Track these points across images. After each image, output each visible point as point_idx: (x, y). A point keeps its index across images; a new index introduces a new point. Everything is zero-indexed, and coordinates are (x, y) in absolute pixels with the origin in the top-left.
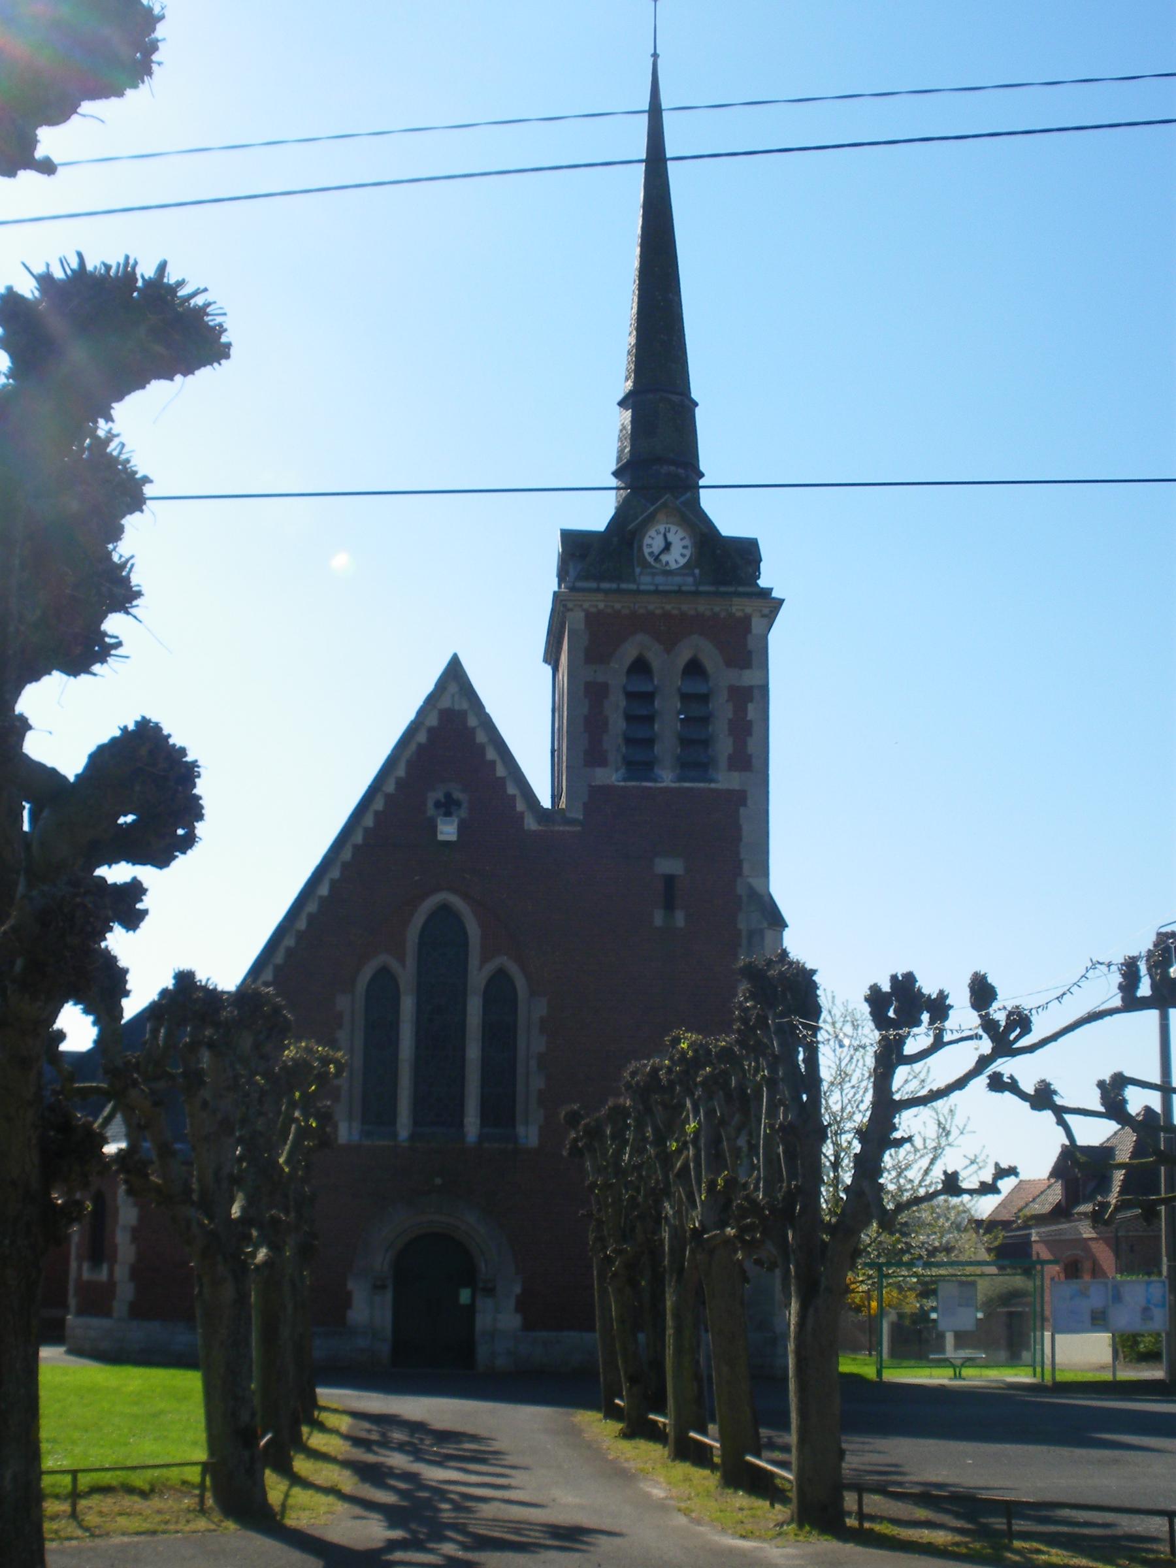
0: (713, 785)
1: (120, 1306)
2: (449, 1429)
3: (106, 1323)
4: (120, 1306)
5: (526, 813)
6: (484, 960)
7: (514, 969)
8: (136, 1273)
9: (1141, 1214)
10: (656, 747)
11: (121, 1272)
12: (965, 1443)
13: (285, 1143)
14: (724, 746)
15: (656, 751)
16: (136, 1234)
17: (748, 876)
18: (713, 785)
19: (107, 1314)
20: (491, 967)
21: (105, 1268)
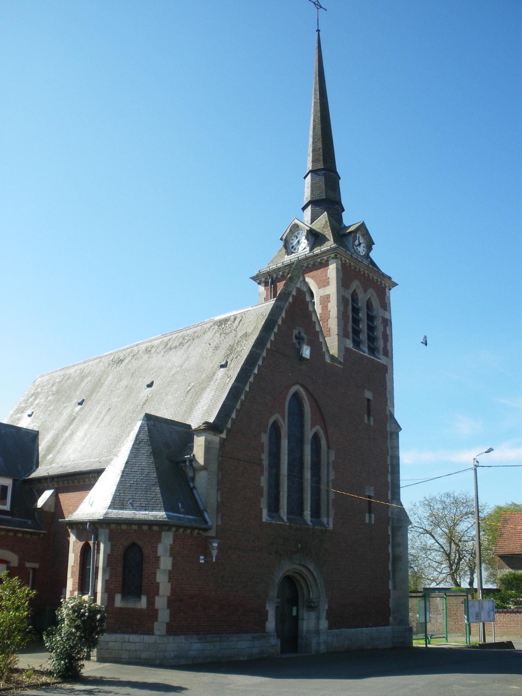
0: (379, 360)
1: (160, 627)
2: (141, 689)
3: (147, 639)
4: (160, 627)
5: (326, 352)
6: (312, 426)
7: (322, 434)
8: (171, 603)
9: (27, 617)
10: (361, 336)
11: (161, 603)
12: (372, 678)
13: (388, 489)
14: (381, 343)
15: (361, 338)
16: (172, 576)
17: (389, 406)
18: (379, 360)
19: (150, 632)
20: (314, 430)
21: (144, 599)
